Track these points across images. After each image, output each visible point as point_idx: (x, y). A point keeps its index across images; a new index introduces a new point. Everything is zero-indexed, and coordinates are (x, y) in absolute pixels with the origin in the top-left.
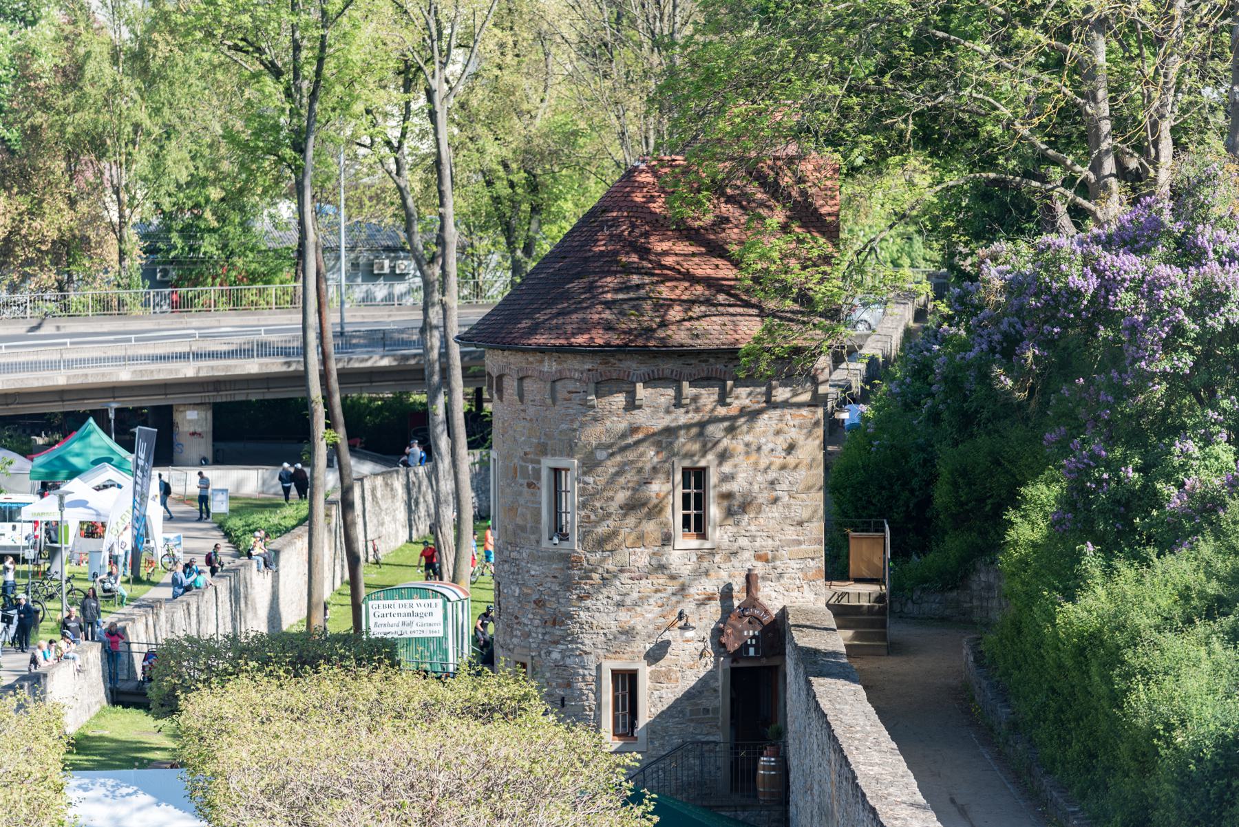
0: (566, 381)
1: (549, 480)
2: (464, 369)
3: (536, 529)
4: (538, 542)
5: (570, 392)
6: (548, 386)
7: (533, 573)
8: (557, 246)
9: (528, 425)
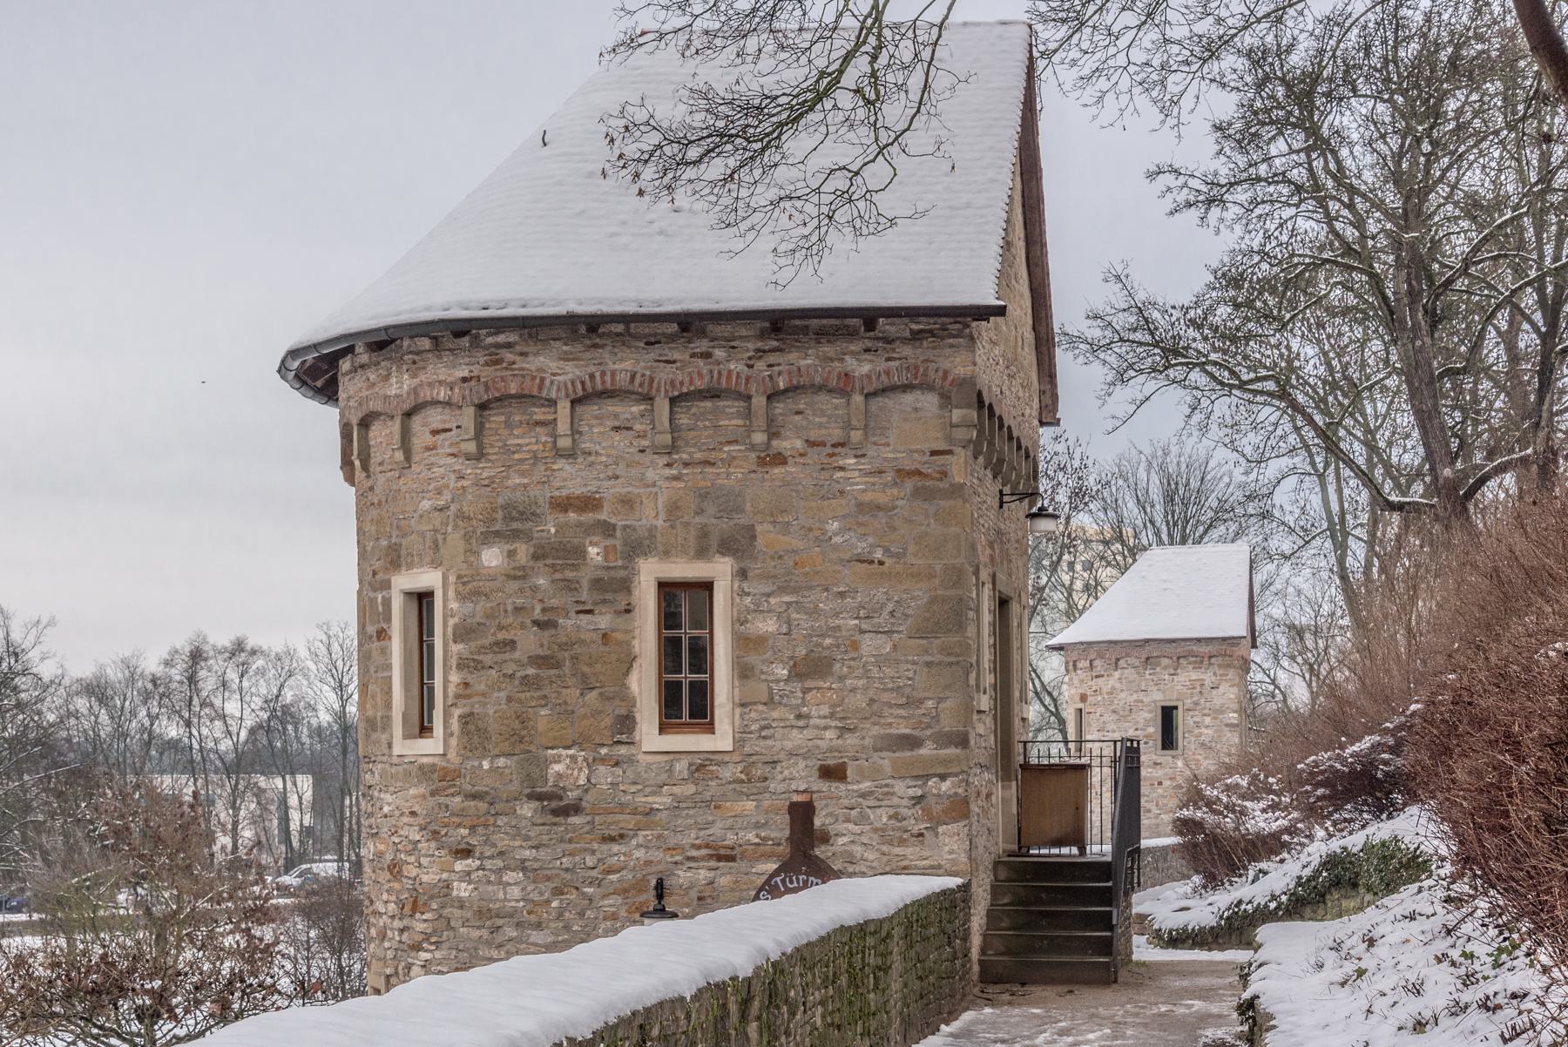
0: (424, 413)
1: (405, 618)
2: (739, 621)
4: (390, 746)
5: (435, 432)
7: (386, 809)
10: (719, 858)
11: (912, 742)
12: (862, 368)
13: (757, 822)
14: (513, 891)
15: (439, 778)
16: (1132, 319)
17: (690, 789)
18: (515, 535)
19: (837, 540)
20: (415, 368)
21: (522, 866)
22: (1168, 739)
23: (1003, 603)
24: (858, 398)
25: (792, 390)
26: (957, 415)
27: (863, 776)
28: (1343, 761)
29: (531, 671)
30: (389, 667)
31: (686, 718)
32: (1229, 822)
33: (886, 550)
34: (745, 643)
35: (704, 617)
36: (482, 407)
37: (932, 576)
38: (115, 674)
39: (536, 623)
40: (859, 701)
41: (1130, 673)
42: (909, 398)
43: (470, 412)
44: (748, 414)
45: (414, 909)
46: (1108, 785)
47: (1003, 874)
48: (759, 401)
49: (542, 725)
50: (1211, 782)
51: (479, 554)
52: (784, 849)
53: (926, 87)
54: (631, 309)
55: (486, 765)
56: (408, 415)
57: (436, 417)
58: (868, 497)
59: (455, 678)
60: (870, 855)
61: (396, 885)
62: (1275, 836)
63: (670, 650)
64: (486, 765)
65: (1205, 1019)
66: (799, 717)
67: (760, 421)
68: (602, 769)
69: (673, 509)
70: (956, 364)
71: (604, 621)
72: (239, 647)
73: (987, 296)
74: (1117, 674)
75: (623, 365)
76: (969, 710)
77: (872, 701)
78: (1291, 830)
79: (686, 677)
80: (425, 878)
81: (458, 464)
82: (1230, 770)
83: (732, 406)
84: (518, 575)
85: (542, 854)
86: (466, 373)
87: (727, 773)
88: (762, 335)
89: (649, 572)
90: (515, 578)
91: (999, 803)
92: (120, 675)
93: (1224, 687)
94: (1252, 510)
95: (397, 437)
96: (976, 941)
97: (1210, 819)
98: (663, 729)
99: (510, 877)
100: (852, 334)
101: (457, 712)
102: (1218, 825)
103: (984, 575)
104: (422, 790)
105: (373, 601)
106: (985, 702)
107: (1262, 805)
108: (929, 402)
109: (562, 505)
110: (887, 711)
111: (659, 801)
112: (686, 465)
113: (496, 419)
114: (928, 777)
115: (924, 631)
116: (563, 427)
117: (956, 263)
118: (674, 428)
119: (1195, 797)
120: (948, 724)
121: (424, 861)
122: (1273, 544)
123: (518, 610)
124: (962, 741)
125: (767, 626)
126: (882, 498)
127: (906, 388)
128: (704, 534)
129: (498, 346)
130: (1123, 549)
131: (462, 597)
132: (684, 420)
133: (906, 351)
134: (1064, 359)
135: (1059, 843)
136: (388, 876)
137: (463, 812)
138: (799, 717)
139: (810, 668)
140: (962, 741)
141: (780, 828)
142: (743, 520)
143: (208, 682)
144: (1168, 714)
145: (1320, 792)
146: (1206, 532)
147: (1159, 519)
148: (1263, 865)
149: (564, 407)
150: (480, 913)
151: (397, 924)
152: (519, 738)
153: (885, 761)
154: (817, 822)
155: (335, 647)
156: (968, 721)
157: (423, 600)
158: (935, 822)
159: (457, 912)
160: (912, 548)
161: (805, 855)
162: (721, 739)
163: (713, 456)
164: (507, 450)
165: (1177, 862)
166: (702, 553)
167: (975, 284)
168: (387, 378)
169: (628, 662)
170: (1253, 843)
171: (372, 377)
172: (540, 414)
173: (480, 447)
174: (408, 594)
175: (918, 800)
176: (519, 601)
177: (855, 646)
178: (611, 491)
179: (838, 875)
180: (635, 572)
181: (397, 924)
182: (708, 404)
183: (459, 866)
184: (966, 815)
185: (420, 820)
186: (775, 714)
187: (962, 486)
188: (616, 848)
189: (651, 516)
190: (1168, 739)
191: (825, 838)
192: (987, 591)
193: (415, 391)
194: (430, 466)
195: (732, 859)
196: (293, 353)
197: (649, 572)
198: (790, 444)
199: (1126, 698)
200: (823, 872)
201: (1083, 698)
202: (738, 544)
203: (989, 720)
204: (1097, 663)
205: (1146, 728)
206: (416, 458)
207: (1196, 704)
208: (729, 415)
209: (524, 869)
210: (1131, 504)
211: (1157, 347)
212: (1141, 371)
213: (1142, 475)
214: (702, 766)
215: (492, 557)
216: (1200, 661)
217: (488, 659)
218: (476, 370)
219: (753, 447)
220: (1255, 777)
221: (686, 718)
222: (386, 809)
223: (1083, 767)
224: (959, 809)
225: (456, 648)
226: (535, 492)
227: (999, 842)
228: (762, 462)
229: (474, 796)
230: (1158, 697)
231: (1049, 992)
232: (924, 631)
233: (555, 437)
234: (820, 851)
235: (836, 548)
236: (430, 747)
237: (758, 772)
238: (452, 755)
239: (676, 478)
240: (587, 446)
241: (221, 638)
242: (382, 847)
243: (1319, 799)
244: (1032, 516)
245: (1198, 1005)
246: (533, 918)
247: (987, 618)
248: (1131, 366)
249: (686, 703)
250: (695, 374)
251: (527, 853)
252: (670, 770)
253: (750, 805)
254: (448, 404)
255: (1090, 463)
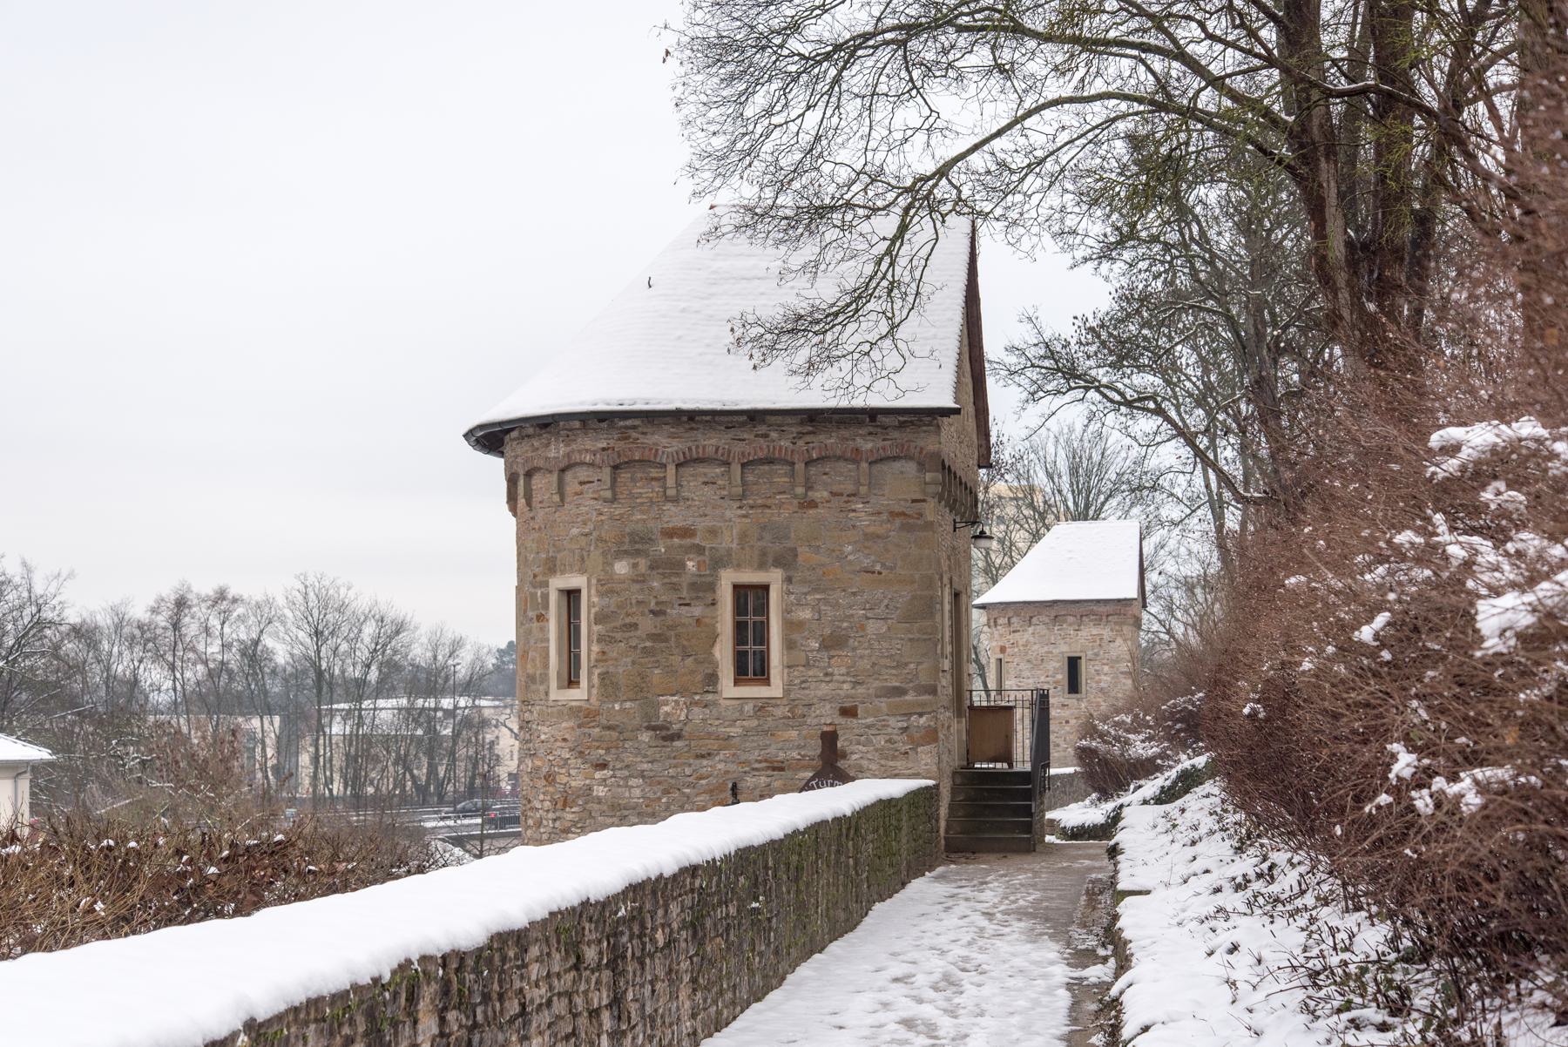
0: (578, 469)
1: (559, 607)
2: (787, 611)
3: (545, 678)
4: (547, 694)
5: (581, 483)
6: (554, 477)
7: (543, 737)
8: (970, 567)
9: (536, 535)
10: (774, 769)
11: (900, 692)
12: (867, 445)
13: (799, 744)
14: (636, 792)
15: (584, 715)
16: (1042, 352)
17: (755, 723)
18: (638, 553)
19: (851, 557)
20: (568, 440)
21: (642, 775)
22: (1074, 686)
23: (957, 595)
24: (864, 465)
25: (821, 459)
26: (929, 476)
27: (868, 714)
28: (1193, 704)
29: (648, 644)
30: (548, 640)
31: (751, 675)
32: (1116, 749)
33: (883, 565)
34: (790, 626)
35: (763, 608)
36: (615, 468)
37: (913, 582)
38: (104, 620)
39: (652, 612)
40: (865, 664)
41: (1041, 629)
42: (897, 465)
43: (608, 470)
44: (792, 475)
45: (565, 805)
46: (1027, 722)
47: (958, 781)
48: (800, 467)
49: (655, 680)
50: (1105, 719)
51: (612, 565)
52: (818, 763)
53: (918, 293)
54: (719, 407)
55: (617, 707)
56: (563, 471)
57: (583, 473)
58: (871, 529)
59: (595, 648)
60: (873, 766)
61: (551, 789)
62: (1151, 760)
63: (740, 628)
64: (617, 707)
65: (1091, 869)
66: (826, 674)
67: (800, 479)
68: (696, 710)
69: (743, 536)
70: (929, 444)
71: (697, 611)
72: (221, 596)
73: (949, 402)
74: (1031, 630)
75: (711, 441)
76: (937, 670)
77: (874, 664)
78: (1163, 756)
79: (750, 647)
80: (573, 784)
81: (598, 505)
82: (1118, 712)
83: (782, 469)
84: (640, 580)
85: (655, 766)
86: (605, 445)
87: (779, 712)
88: (802, 423)
89: (727, 580)
90: (638, 582)
91: (955, 730)
92: (109, 622)
93: (1119, 641)
94: (1142, 488)
95: (555, 485)
96: (943, 824)
97: (1102, 747)
98: (737, 683)
99: (632, 782)
100: (861, 423)
101: (596, 672)
102: (1108, 752)
103: (946, 580)
104: (571, 724)
105: (533, 596)
106: (946, 664)
107: (1141, 737)
108: (910, 468)
109: (669, 533)
110: (884, 671)
111: (734, 731)
112: (752, 507)
113: (625, 476)
114: (911, 714)
115: (909, 618)
116: (671, 482)
117: (933, 387)
118: (744, 483)
119: (1090, 730)
120: (924, 680)
121: (573, 772)
122: (1164, 513)
123: (639, 603)
124: (933, 690)
125: (805, 614)
126: (880, 531)
127: (895, 458)
128: (764, 554)
129: (627, 427)
130: (1040, 520)
131: (601, 594)
132: (750, 478)
133: (896, 434)
134: (990, 382)
135: (995, 760)
136: (544, 782)
137: (599, 738)
138: (826, 674)
139: (833, 643)
140: (933, 690)
141: (815, 748)
142: (789, 544)
143: (191, 628)
144: (1073, 664)
145: (1178, 726)
146: (1106, 500)
147: (1066, 487)
148: (1142, 782)
149: (671, 469)
150: (613, 807)
151: (551, 815)
152: (639, 689)
153: (883, 703)
154: (839, 745)
155: (312, 595)
156: (937, 679)
157: (572, 595)
158: (916, 744)
159: (596, 807)
160: (899, 563)
161: (831, 767)
162: (775, 690)
163: (769, 502)
164: (632, 497)
165: (1081, 784)
166: (762, 566)
167: (943, 397)
168: (548, 445)
169: (713, 638)
170: (1134, 765)
171: (536, 444)
172: (654, 473)
173: (614, 494)
174: (561, 591)
175: (905, 730)
176: (640, 597)
177: (863, 627)
178: (701, 524)
179: (853, 779)
180: (717, 578)
181: (551, 815)
182: (766, 468)
183: (598, 775)
184: (936, 740)
185: (570, 744)
186: (811, 673)
187: (932, 523)
188: (705, 762)
189: (729, 541)
190: (1074, 686)
191: (844, 756)
192: (947, 590)
193: (568, 455)
194: (578, 506)
195: (782, 769)
196: (481, 427)
197: (727, 580)
198: (820, 494)
199: (1038, 649)
200: (843, 778)
201: (1003, 650)
202: (785, 561)
203: (948, 676)
204: (1014, 620)
205: (1052, 676)
206: (568, 499)
207: (1097, 655)
208: (780, 476)
209: (643, 777)
210: (1042, 475)
211: (1060, 369)
212: (1048, 393)
213: (1051, 449)
214: (762, 707)
215: (621, 568)
216: (1100, 619)
217: (618, 636)
218: (612, 443)
219: (795, 497)
220: (1136, 716)
221: (751, 675)
222: (543, 737)
223: (1011, 708)
224: (931, 736)
225: (596, 628)
226: (651, 524)
227: (955, 761)
228: (801, 506)
229: (609, 728)
230: (1065, 649)
231: (992, 857)
232: (909, 618)
233: (665, 489)
234: (841, 764)
235: (850, 562)
236: (578, 695)
237: (799, 711)
238: (593, 700)
239: (745, 516)
240: (686, 494)
241: (204, 587)
242: (539, 763)
243: (1179, 731)
244: (975, 537)
245: (1087, 862)
246: (649, 810)
247: (947, 607)
248: (1040, 388)
249: (751, 667)
250: (759, 448)
251: (645, 766)
252: (741, 711)
253: (794, 733)
254: (592, 465)
255: (1005, 440)
